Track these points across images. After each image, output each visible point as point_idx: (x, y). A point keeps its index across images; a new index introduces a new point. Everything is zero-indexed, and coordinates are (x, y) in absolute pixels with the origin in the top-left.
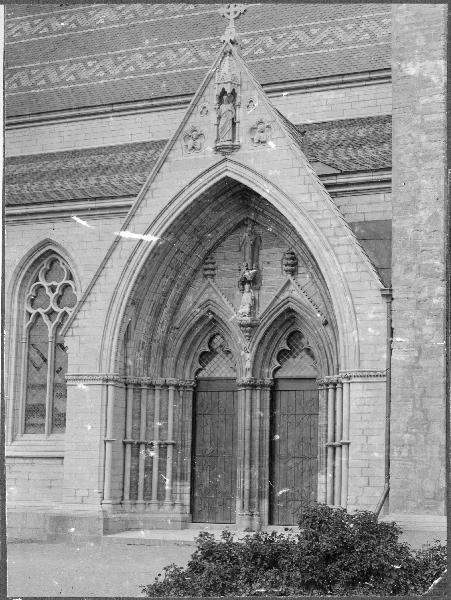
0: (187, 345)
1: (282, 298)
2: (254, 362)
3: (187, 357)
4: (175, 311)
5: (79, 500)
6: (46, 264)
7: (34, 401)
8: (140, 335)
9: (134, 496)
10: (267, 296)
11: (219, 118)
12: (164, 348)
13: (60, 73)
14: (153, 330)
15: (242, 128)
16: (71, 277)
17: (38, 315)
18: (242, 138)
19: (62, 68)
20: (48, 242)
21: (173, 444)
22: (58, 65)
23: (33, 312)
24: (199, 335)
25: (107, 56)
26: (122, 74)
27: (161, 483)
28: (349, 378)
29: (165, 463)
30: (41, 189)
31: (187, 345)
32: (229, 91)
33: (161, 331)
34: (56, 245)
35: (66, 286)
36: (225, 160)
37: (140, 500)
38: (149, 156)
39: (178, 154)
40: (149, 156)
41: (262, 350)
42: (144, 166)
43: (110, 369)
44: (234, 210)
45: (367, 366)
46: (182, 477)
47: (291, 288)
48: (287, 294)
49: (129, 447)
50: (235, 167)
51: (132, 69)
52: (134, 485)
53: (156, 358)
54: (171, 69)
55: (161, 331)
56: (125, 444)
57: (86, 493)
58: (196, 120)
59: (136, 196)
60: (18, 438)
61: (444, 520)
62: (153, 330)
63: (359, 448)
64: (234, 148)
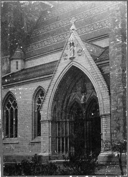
1: (74, 98)
5: (44, 152)
6: (40, 93)
7: (12, 135)
8: (59, 109)
10: (88, 96)
11: (70, 50)
15: (76, 51)
18: (76, 55)
20: (40, 87)
21: (69, 137)
23: (38, 105)
25: (64, 34)
27: (66, 147)
28: (102, 116)
30: (11, 79)
32: (71, 43)
34: (42, 88)
36: (72, 61)
37: (61, 152)
39: (63, 61)
43: (50, 118)
45: (106, 113)
48: (75, 97)
49: (57, 138)
50: (75, 63)
54: (95, 30)
55: (64, 107)
56: (56, 137)
57: (45, 150)
58: (66, 51)
59: (53, 73)
60: (36, 137)
63: (104, 135)
64: (74, 58)
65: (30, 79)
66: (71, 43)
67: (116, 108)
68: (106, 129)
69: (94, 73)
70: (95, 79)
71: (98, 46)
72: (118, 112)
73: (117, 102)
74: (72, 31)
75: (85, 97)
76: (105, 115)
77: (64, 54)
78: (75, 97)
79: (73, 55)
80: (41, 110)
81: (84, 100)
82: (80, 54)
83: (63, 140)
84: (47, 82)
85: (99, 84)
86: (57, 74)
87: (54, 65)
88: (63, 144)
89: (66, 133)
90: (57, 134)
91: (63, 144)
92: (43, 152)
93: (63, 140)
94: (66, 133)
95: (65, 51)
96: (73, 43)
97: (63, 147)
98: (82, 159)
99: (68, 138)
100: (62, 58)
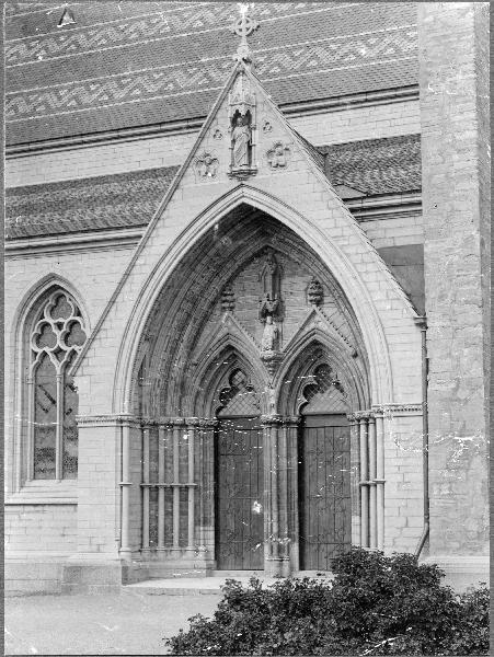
1: (307, 329)
5: (95, 548)
6: (51, 301)
8: (155, 373)
10: (290, 329)
11: (234, 141)
12: (182, 385)
14: (169, 369)
18: (259, 162)
20: (53, 276)
23: (40, 351)
32: (243, 113)
33: (178, 366)
34: (61, 279)
43: (124, 408)
44: (251, 241)
45: (401, 400)
46: (205, 522)
48: (312, 325)
53: (173, 397)
55: (178, 366)
56: (142, 488)
60: (27, 483)
62: (169, 369)
65: (64, 234)
66: (243, 113)
67: (453, 385)
68: (400, 462)
69: (346, 243)
70: (354, 265)
71: (138, 173)
72: (459, 400)
73: (458, 359)
74: (243, 63)
75: (278, 335)
76: (399, 411)
77: (200, 153)
78: (312, 325)
79: (245, 160)
80: (79, 373)
81: (276, 343)
82: (282, 160)
83: (169, 499)
84: (117, 260)
85: (373, 286)
86: (161, 232)
87: (162, 182)
88: (169, 514)
89: (183, 470)
90: (146, 474)
91: (169, 514)
92: (87, 548)
93: (169, 499)
94: (183, 470)
95: (204, 144)
96: (248, 114)
97: (168, 530)
98: (468, 620)
99: (176, 491)
100: (190, 169)
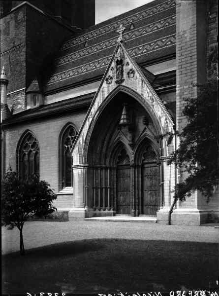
0: (114, 154)
2: (135, 159)
3: (114, 158)
4: (109, 143)
9: (97, 205)
13: (82, 69)
16: (36, 140)
17: (68, 147)
19: (82, 68)
20: (69, 123)
22: (81, 67)
24: (117, 151)
26: (101, 66)
29: (98, 192)
31: (114, 154)
34: (73, 124)
35: (35, 143)
38: (92, 97)
40: (92, 97)
41: (137, 156)
42: (92, 98)
47: (146, 130)
48: (145, 133)
51: (103, 64)
52: (97, 202)
56: (93, 188)
61: (217, 231)
